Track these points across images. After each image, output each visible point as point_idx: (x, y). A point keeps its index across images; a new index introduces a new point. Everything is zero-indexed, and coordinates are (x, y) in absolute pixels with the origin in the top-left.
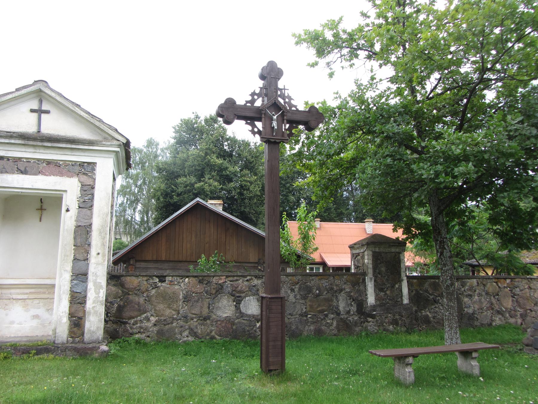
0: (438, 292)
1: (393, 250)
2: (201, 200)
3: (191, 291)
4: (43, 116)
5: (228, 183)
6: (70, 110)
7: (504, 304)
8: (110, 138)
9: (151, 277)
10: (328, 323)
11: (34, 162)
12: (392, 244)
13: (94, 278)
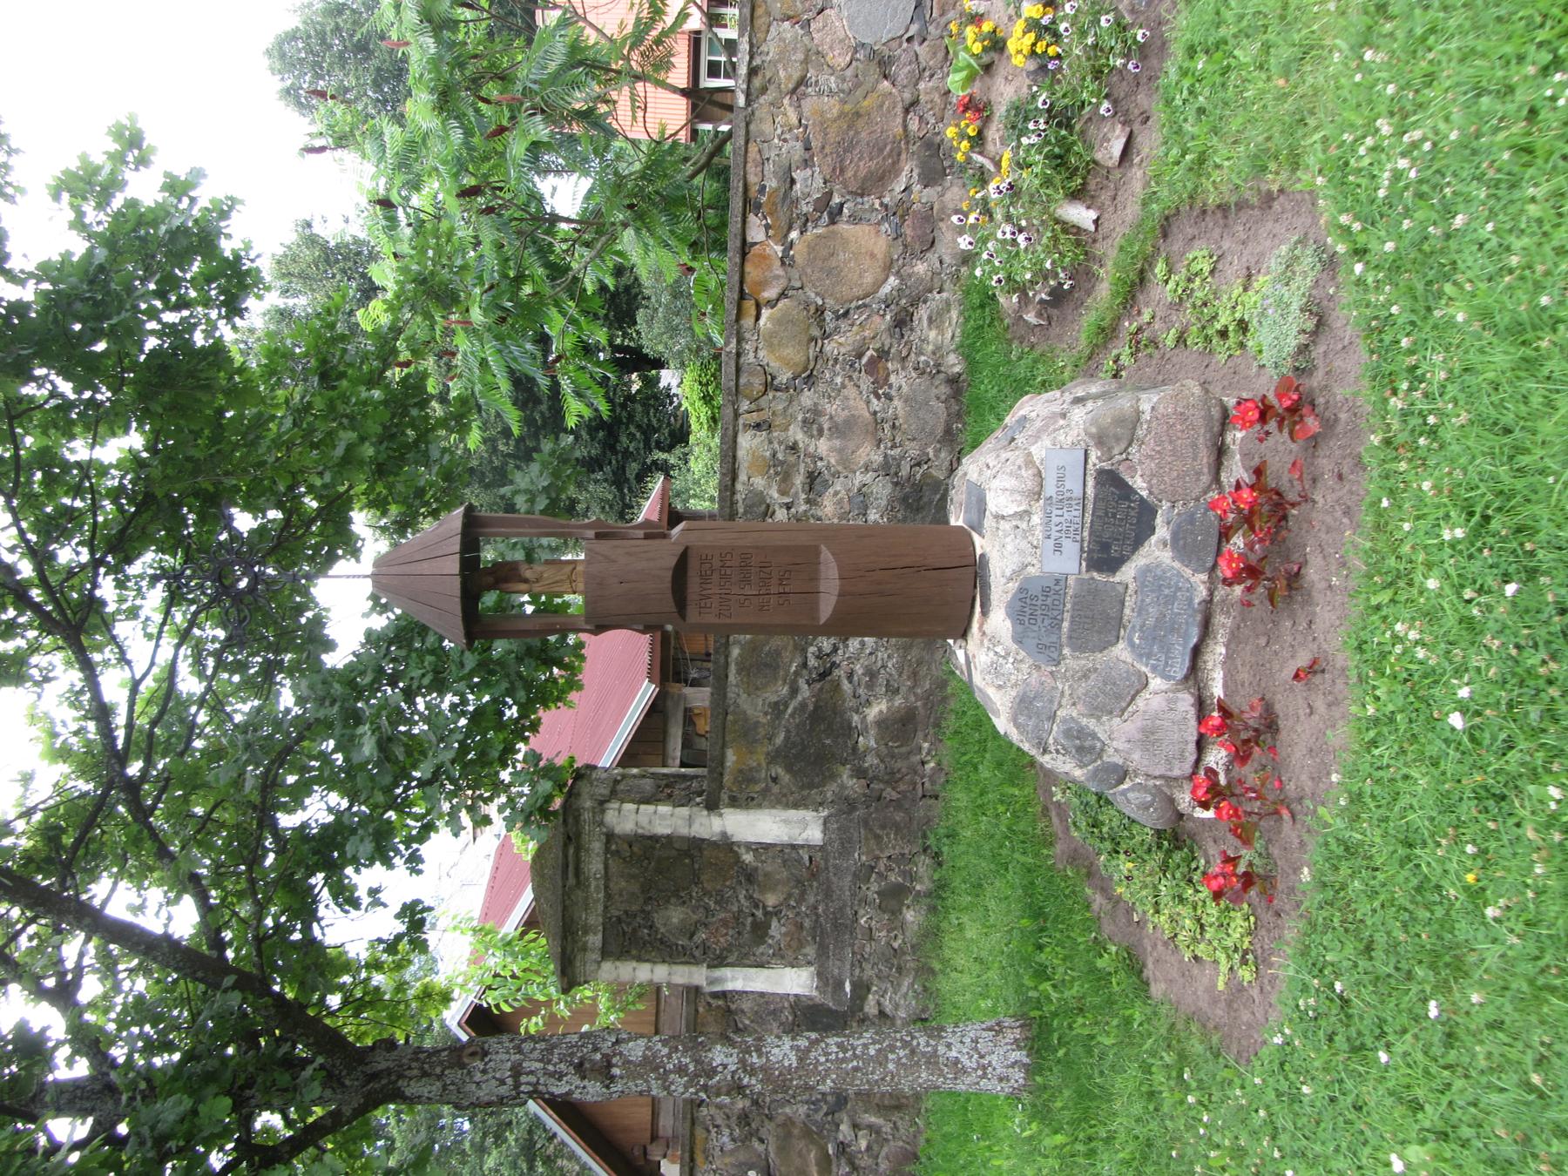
0: (786, 655)
1: (594, 866)
7: (868, 279)
10: (869, 1148)
12: (572, 881)
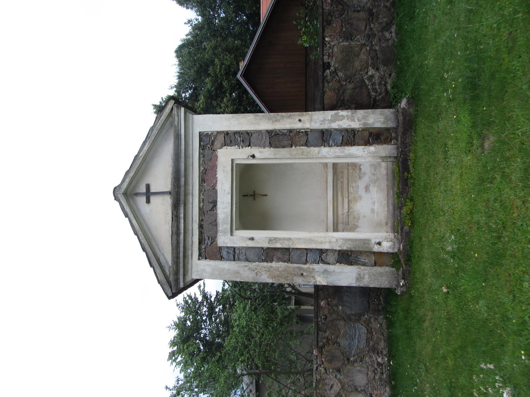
2: (240, 73)
3: (340, 33)
4: (152, 190)
5: (224, 88)
6: (142, 164)
8: (171, 119)
9: (324, 78)
11: (203, 195)
13: (326, 122)
